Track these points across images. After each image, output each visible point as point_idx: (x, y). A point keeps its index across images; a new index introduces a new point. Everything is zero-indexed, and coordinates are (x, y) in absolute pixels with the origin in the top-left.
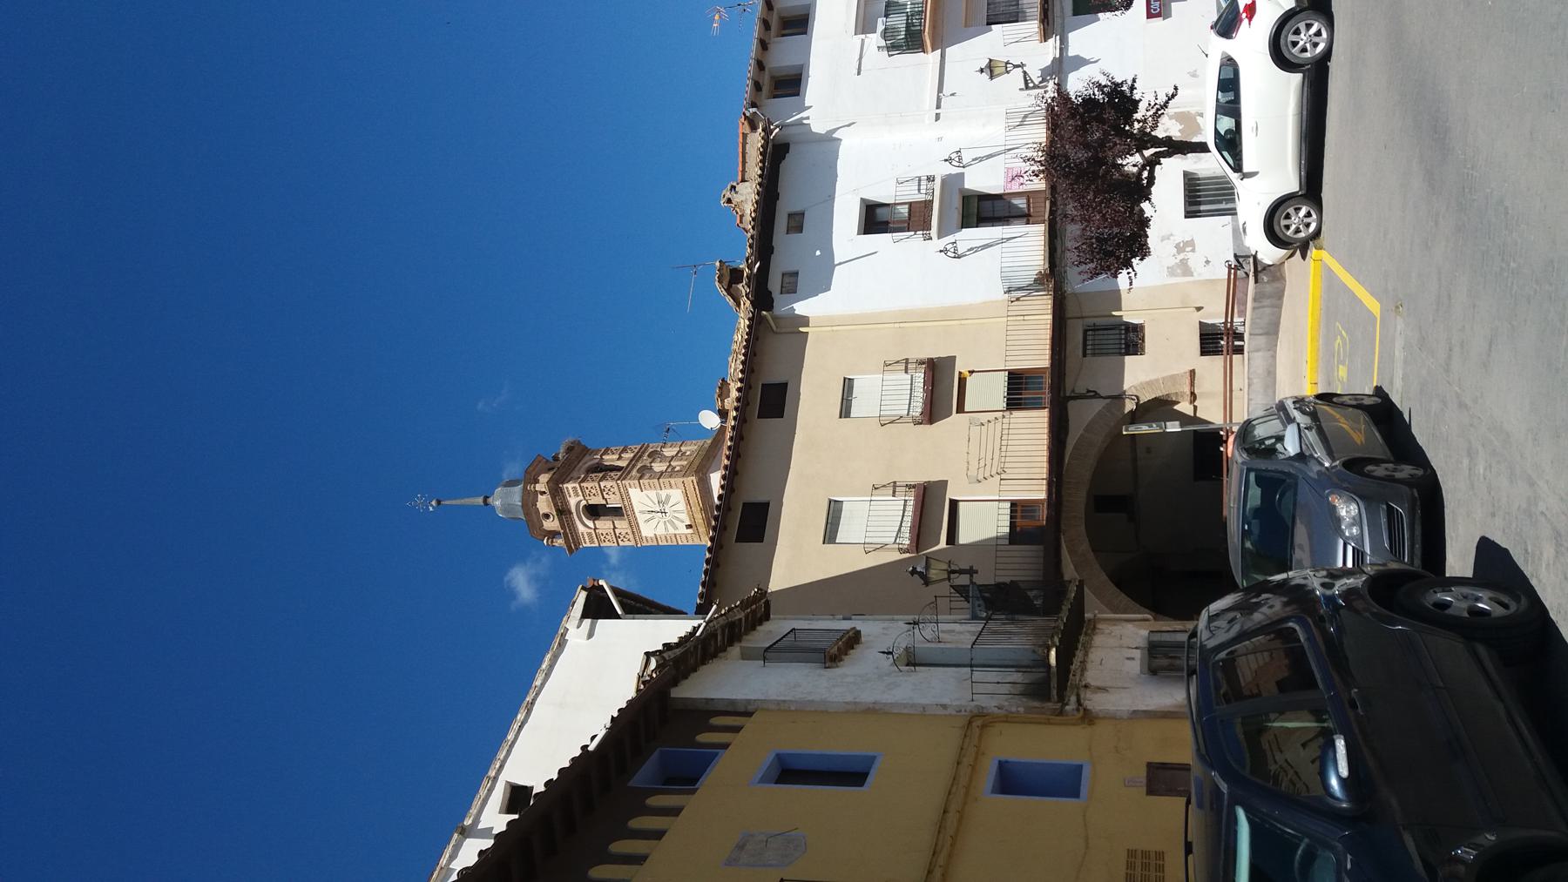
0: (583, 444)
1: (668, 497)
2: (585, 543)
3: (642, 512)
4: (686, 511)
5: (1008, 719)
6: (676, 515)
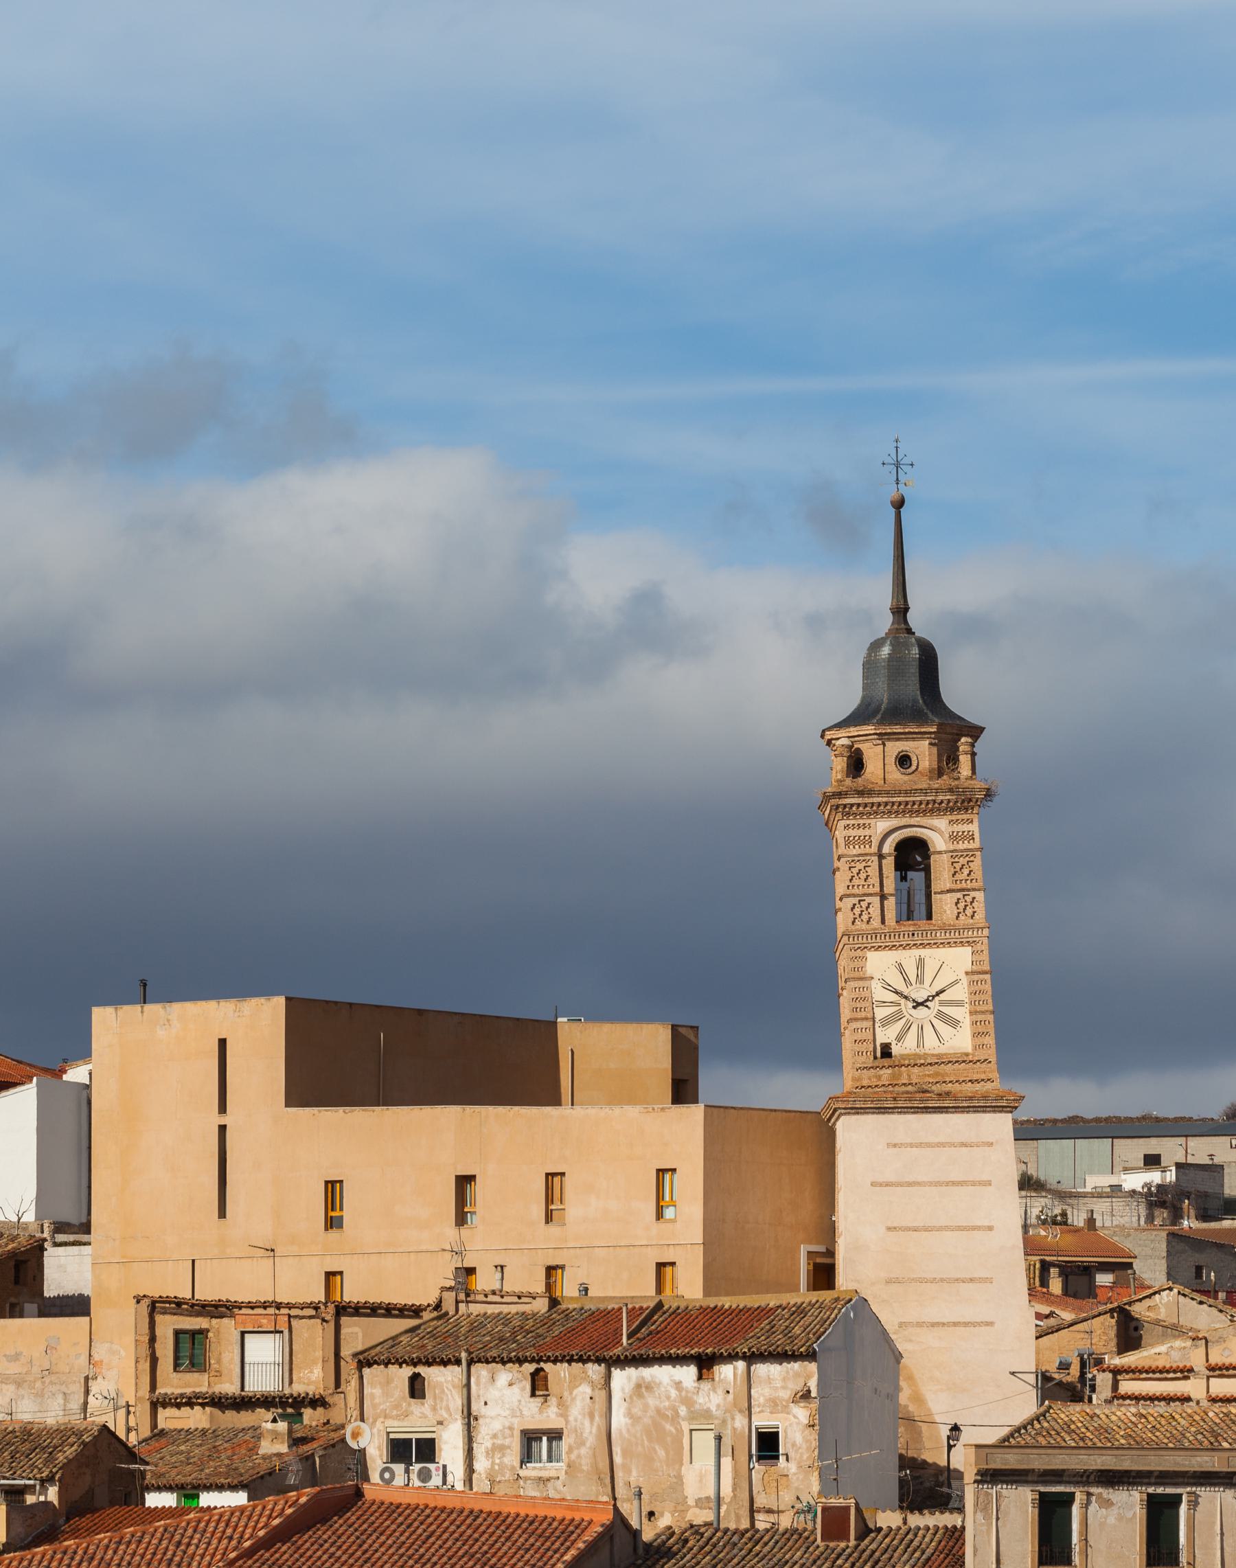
0: (703, 1496)
1: (953, 1023)
2: (847, 827)
3: (921, 963)
4: (920, 1051)
5: (693, 1507)
6: (914, 1029)
